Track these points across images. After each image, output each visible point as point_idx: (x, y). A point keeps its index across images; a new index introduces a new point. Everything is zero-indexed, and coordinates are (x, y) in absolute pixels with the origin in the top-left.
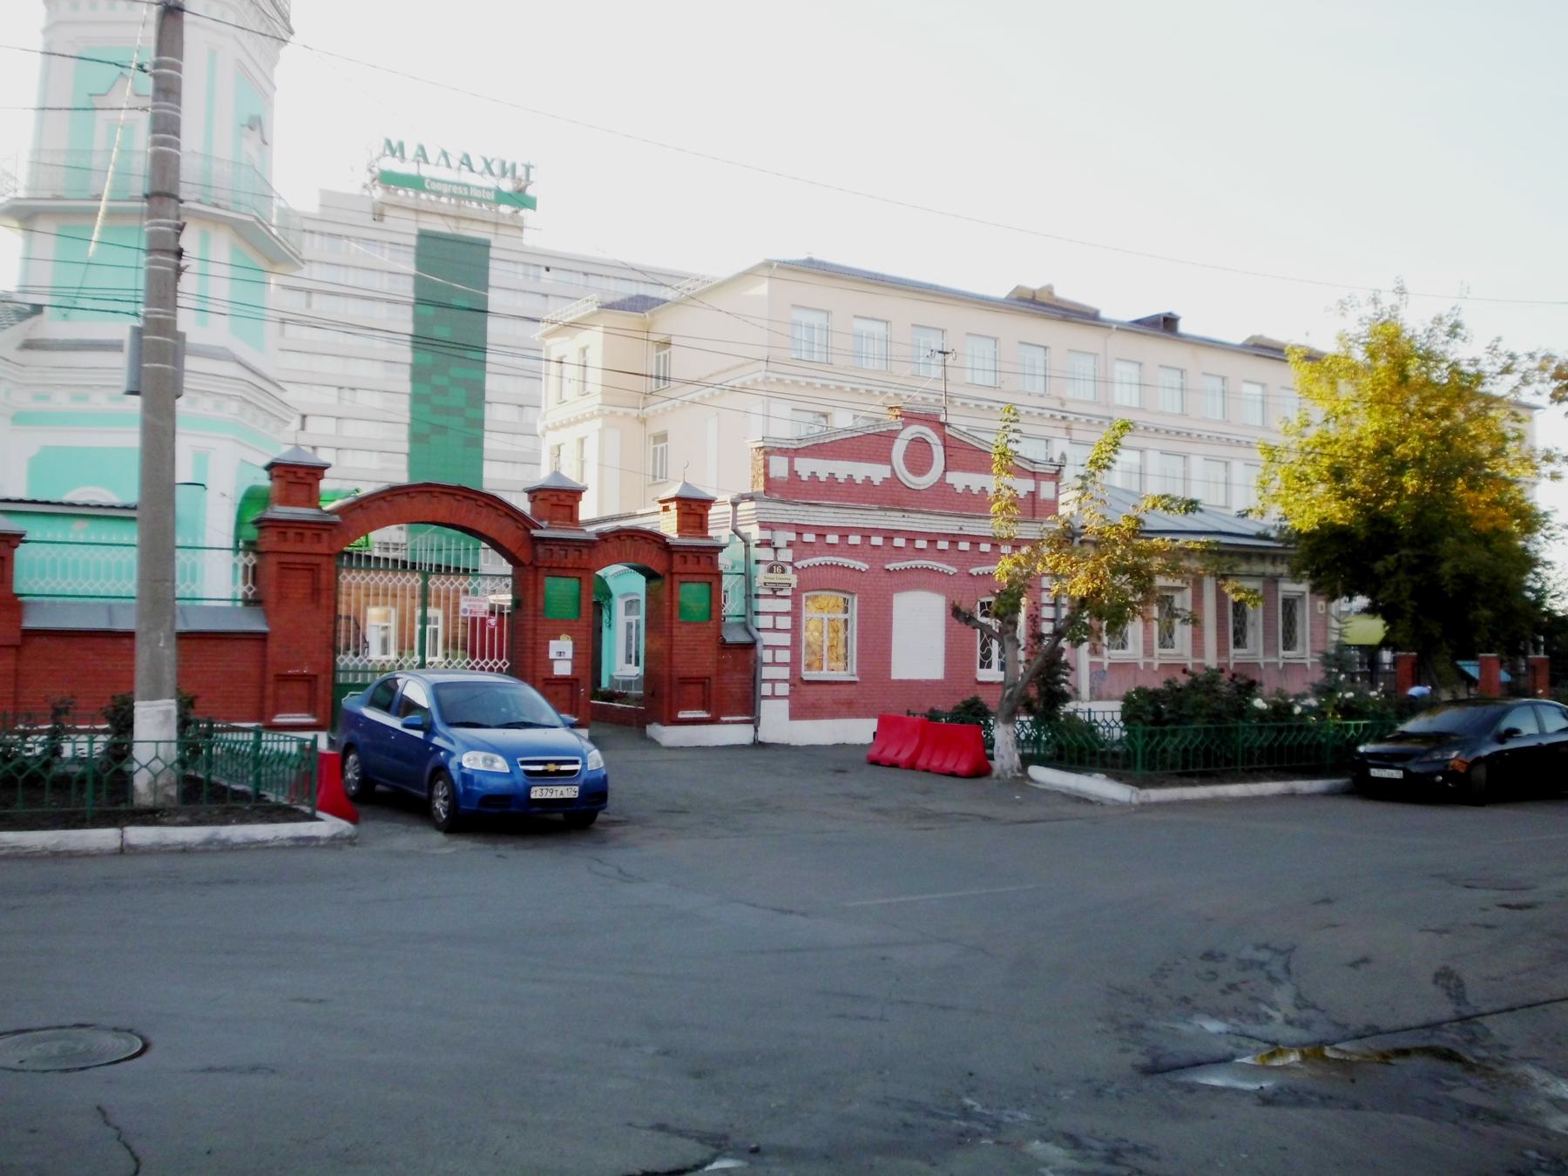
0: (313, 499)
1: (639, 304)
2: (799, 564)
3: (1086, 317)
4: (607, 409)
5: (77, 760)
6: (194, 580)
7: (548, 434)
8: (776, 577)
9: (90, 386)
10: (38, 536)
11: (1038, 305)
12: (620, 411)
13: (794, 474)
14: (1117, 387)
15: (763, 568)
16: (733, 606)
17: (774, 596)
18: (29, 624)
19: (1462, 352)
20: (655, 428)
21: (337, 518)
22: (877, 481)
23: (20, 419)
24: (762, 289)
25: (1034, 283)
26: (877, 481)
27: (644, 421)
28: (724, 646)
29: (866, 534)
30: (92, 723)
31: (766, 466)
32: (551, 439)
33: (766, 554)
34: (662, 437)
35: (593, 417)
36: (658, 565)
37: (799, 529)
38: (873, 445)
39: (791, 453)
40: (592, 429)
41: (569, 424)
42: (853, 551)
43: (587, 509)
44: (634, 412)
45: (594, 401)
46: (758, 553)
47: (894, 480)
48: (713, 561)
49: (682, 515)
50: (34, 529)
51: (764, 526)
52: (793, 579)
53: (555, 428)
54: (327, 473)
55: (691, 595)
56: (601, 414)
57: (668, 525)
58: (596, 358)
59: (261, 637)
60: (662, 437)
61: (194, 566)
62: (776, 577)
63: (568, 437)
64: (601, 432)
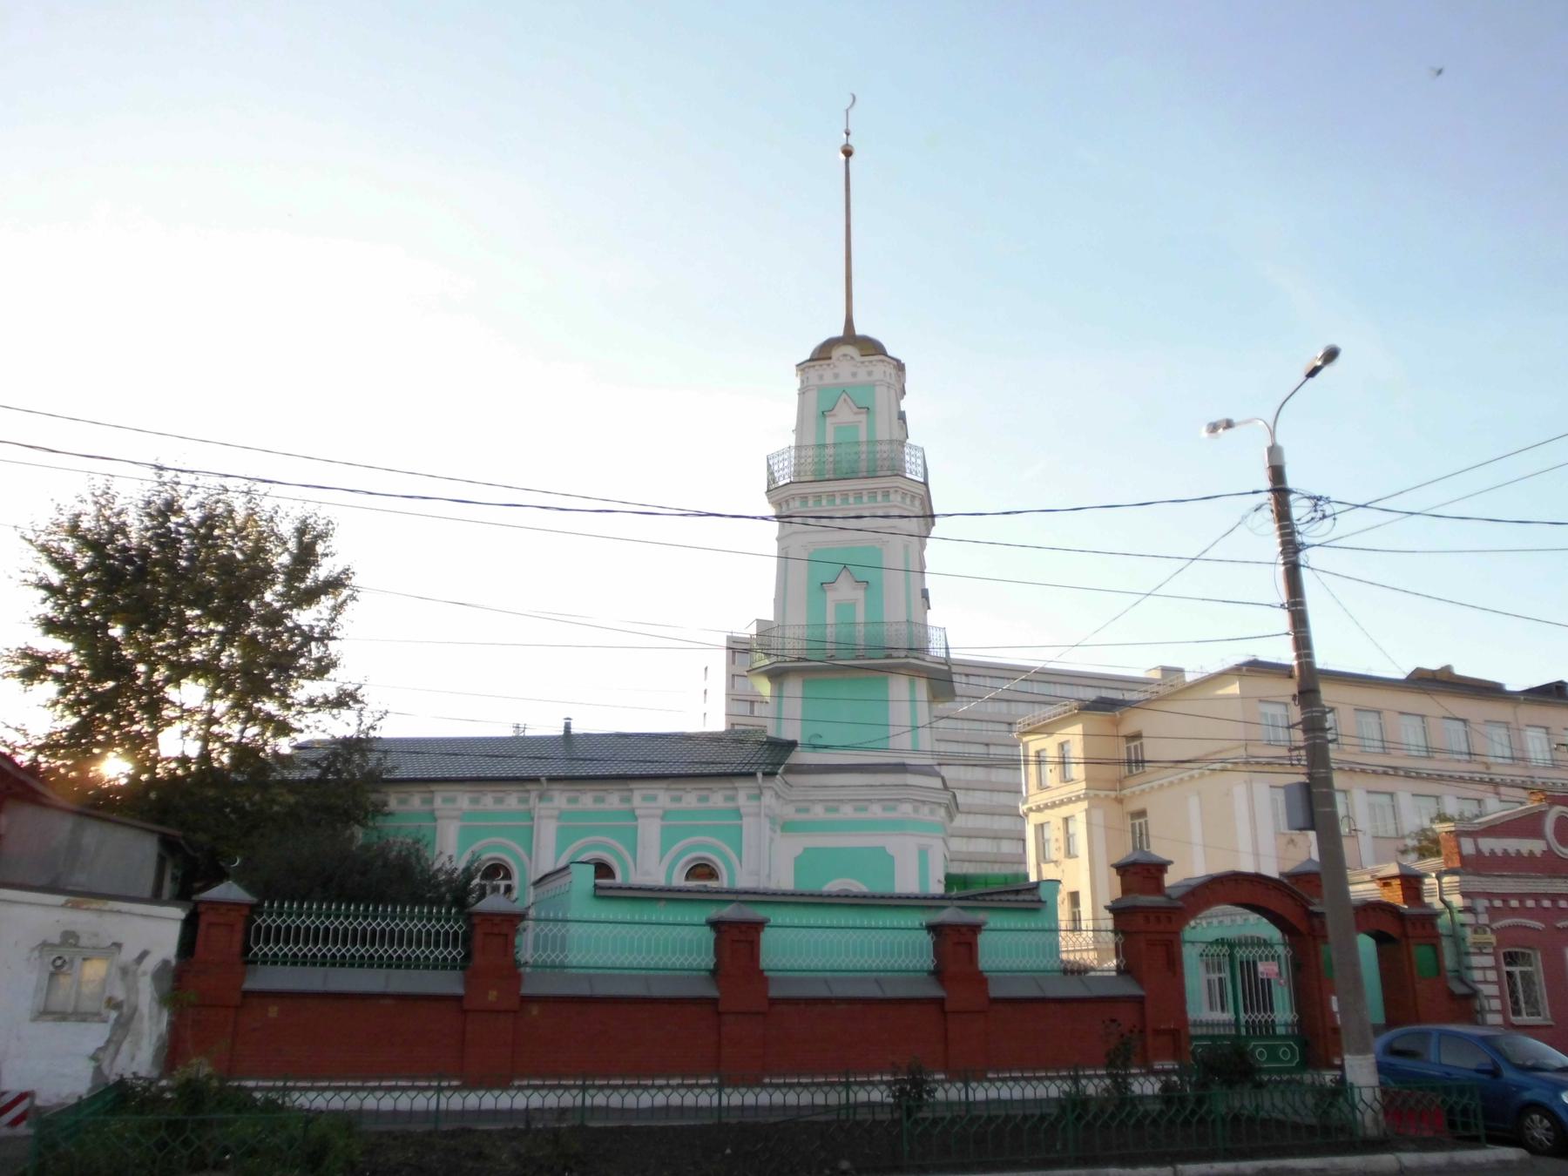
0: (1159, 887)
1: (1104, 705)
2: (1495, 926)
3: (1488, 691)
4: (1092, 793)
5: (949, 1104)
6: (563, 951)
7: (1032, 815)
8: (1481, 938)
9: (841, 801)
10: (780, 921)
11: (1435, 683)
12: (1102, 794)
13: (1478, 851)
14: (798, 715)
15: (1468, 931)
16: (1449, 962)
17: (1481, 954)
18: (526, 990)
19: (830, 633)
20: (1136, 806)
21: (1180, 904)
22: (1538, 853)
23: (787, 827)
24: (1234, 689)
25: (1433, 664)
26: (1538, 853)
27: (1120, 801)
28: (1452, 996)
29: (1537, 897)
30: (826, 1076)
31: (1459, 846)
32: (1034, 819)
33: (1466, 918)
34: (1142, 814)
35: (1078, 799)
36: (1391, 928)
37: (1490, 896)
38: (1527, 826)
39: (1473, 835)
40: (1079, 811)
41: (1054, 805)
42: (1523, 911)
43: (1171, 879)
44: (1113, 794)
45: (1080, 787)
46: (1461, 918)
47: (1549, 853)
48: (1434, 926)
49: (1404, 888)
50: (776, 916)
51: (1465, 895)
52: (1492, 939)
53: (1039, 809)
54: (1170, 868)
55: (1421, 953)
56: (1087, 797)
57: (1395, 896)
58: (1076, 750)
59: (1140, 1000)
60: (1142, 814)
61: (563, 938)
62: (1481, 938)
63: (1054, 817)
64: (1088, 811)
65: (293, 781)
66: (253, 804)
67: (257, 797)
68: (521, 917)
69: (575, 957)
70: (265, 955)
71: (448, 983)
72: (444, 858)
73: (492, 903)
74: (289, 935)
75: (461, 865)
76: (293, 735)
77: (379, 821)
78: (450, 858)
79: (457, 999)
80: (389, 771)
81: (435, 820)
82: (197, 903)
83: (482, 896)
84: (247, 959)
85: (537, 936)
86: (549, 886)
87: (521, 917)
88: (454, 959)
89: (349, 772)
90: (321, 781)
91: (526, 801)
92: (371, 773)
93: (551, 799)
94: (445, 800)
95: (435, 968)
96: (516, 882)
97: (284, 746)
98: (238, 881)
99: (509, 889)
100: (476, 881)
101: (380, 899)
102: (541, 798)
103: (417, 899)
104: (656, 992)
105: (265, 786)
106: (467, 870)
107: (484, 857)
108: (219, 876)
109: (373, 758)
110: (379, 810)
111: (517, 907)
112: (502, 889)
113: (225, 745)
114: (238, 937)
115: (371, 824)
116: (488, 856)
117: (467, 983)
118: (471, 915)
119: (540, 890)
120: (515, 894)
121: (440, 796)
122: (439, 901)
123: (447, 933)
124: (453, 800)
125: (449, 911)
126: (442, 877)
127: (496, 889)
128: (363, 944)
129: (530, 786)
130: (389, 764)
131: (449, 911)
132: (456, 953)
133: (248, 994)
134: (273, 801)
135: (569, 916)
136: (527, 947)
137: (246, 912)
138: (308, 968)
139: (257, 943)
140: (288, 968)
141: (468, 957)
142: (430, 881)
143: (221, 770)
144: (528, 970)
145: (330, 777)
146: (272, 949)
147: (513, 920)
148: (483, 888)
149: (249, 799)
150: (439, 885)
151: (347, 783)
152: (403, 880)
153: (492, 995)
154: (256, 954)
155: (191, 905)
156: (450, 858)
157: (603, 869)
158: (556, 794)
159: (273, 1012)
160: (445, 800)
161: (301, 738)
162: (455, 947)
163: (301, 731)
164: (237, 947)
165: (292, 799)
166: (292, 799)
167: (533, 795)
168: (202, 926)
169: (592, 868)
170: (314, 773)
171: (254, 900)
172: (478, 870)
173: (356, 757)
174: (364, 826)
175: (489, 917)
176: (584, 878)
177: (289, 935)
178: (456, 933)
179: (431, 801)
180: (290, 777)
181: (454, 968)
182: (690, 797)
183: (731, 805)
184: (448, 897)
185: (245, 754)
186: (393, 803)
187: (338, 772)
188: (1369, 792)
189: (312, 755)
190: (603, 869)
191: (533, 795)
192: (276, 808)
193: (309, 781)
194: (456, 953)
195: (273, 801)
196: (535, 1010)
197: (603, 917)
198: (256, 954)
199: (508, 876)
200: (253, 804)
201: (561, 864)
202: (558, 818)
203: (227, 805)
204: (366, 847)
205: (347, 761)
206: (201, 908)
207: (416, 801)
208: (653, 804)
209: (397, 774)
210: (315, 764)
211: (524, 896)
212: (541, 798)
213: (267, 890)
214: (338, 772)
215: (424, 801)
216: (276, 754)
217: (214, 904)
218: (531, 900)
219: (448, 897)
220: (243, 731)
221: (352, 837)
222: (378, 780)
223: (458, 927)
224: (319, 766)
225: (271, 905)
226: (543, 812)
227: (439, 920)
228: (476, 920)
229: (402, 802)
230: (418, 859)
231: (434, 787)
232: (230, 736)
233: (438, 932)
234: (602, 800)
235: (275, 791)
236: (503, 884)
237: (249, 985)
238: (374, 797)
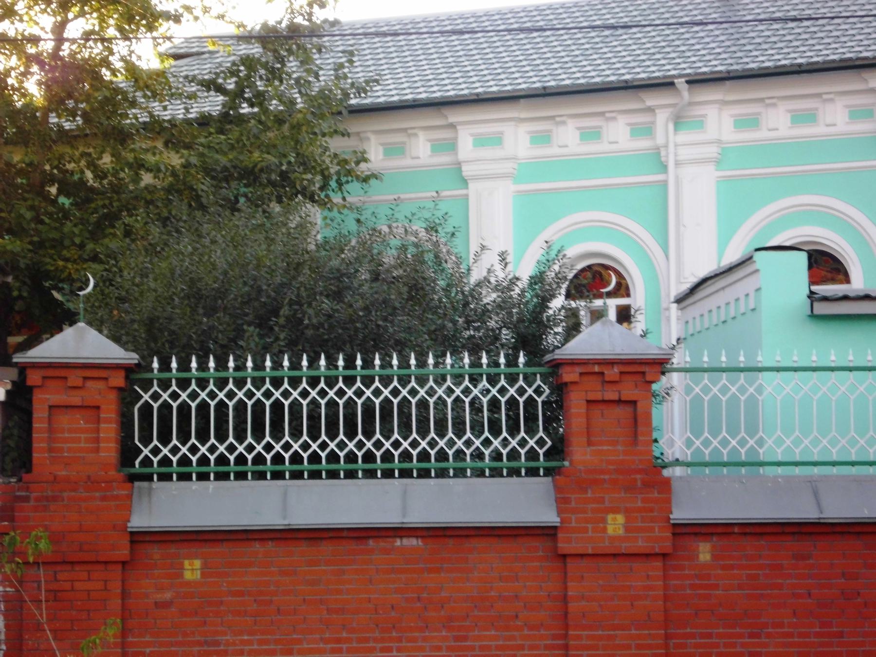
6: (752, 430)
18: (680, 514)
61: (752, 402)
65: (172, 122)
66: (100, 175)
67: (107, 160)
68: (660, 365)
69: (774, 447)
70: (165, 462)
71: (526, 502)
72: (490, 259)
73: (598, 340)
74: (207, 422)
75: (525, 271)
76: (164, 27)
77: (354, 192)
78: (503, 257)
79: (548, 532)
80: (361, 91)
81: (465, 182)
82: (23, 369)
83: (573, 328)
84: (131, 468)
85: (696, 404)
86: (720, 299)
87: (660, 365)
88: (532, 455)
89: (280, 98)
90: (227, 119)
91: (648, 130)
92: (324, 96)
93: (700, 123)
94: (481, 141)
95: (496, 473)
96: (638, 299)
97: (146, 52)
98: (97, 324)
99: (625, 315)
100: (558, 302)
101: (373, 342)
102: (678, 121)
103: (446, 343)
104: (838, 509)
105: (121, 137)
106: (537, 279)
107: (571, 252)
108: (59, 319)
109: (325, 63)
110: (350, 170)
111: (650, 349)
112: (612, 315)
113: (30, 59)
114: (109, 430)
115: (337, 199)
116: (579, 250)
117: (562, 503)
118: (557, 365)
119: (696, 310)
120: (640, 324)
121: (469, 132)
122: (492, 342)
123: (512, 403)
124: (498, 140)
125: (512, 362)
126: (490, 297)
127: (597, 315)
128: (351, 434)
129: (652, 99)
130: (359, 74)
131: (512, 362)
132: (536, 441)
133: (139, 538)
134: (139, 165)
135: (763, 359)
136: (675, 426)
137: (118, 380)
138: (250, 485)
139: (146, 440)
140: (212, 485)
141: (557, 451)
142: (467, 305)
143: (29, 108)
144: (678, 471)
145: (245, 109)
146: (174, 450)
147: (648, 369)
148: (573, 314)
149: (92, 165)
150: (485, 313)
151: (280, 121)
152: (404, 306)
153: (615, 524)
154: (147, 462)
155: (13, 374)
156: (503, 257)
157: (824, 265)
158: (711, 113)
159: (192, 570)
160: (481, 141)
161: (179, 33)
162: (531, 431)
163: (177, 19)
164: (110, 451)
165: (175, 160)
166: (175, 160)
167: (662, 117)
168: (40, 414)
169: (801, 259)
170: (213, 104)
171: (132, 358)
172: (560, 278)
173: (292, 65)
174: (324, 204)
175: (596, 368)
176: (786, 281)
177: (207, 422)
178: (530, 402)
179: (452, 146)
180: (166, 115)
181: (532, 472)
182: (568, 133)
183: (445, 159)
184: (506, 335)
185: (73, 79)
186: (376, 156)
187: (259, 99)
188: (617, 142)
189: (204, 69)
190: (824, 265)
191: (662, 117)
192: (147, 179)
193: (204, 121)
194: (536, 441)
195: (139, 165)
196: (704, 552)
197: (832, 358)
198: (147, 462)
199: (622, 289)
200: (100, 175)
201: (732, 256)
202: (718, 162)
203: (52, 181)
204: (337, 246)
205: (275, 74)
206: (33, 378)
207: (421, 146)
208: (498, 153)
209: (379, 96)
210: (212, 85)
211: (657, 325)
212: (678, 121)
213: (154, 338)
214: (259, 99)
215: (438, 147)
216: (132, 70)
217: (58, 370)
218: (675, 332)
219: (506, 335)
220: (59, 29)
221: (304, 227)
222: (345, 110)
223: (538, 390)
224: (220, 89)
225: (165, 366)
226: (685, 153)
227: (493, 380)
228: (569, 375)
229: (391, 150)
230: (438, 259)
231: (454, 116)
232: (35, 40)
233: (494, 404)
234: (810, 117)
235: (141, 144)
236: (613, 304)
237: (139, 521)
238: (336, 144)
